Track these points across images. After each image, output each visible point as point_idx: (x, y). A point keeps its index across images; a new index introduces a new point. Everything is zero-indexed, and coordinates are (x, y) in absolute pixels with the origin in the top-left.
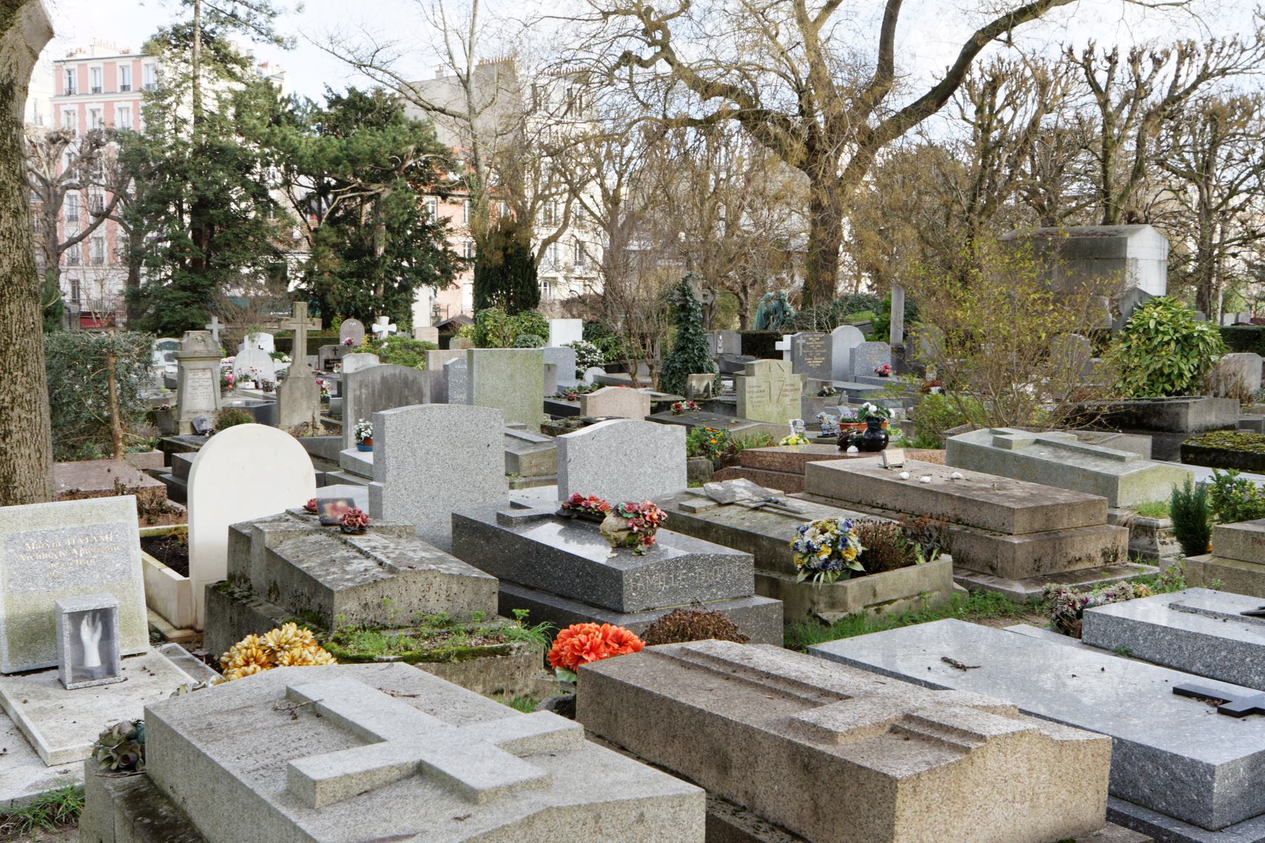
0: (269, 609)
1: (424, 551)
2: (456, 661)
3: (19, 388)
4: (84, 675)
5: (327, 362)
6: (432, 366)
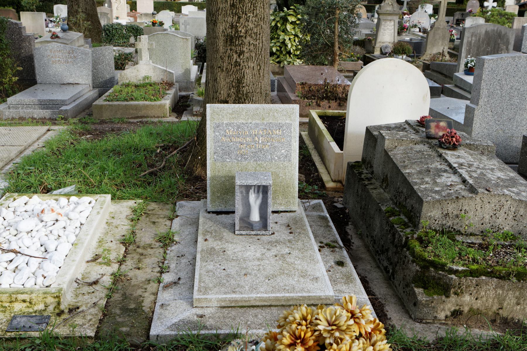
0: (380, 194)
1: (501, 170)
2: (515, 280)
3: (250, 24)
4: (248, 225)
5: (457, 20)
6: (515, 27)
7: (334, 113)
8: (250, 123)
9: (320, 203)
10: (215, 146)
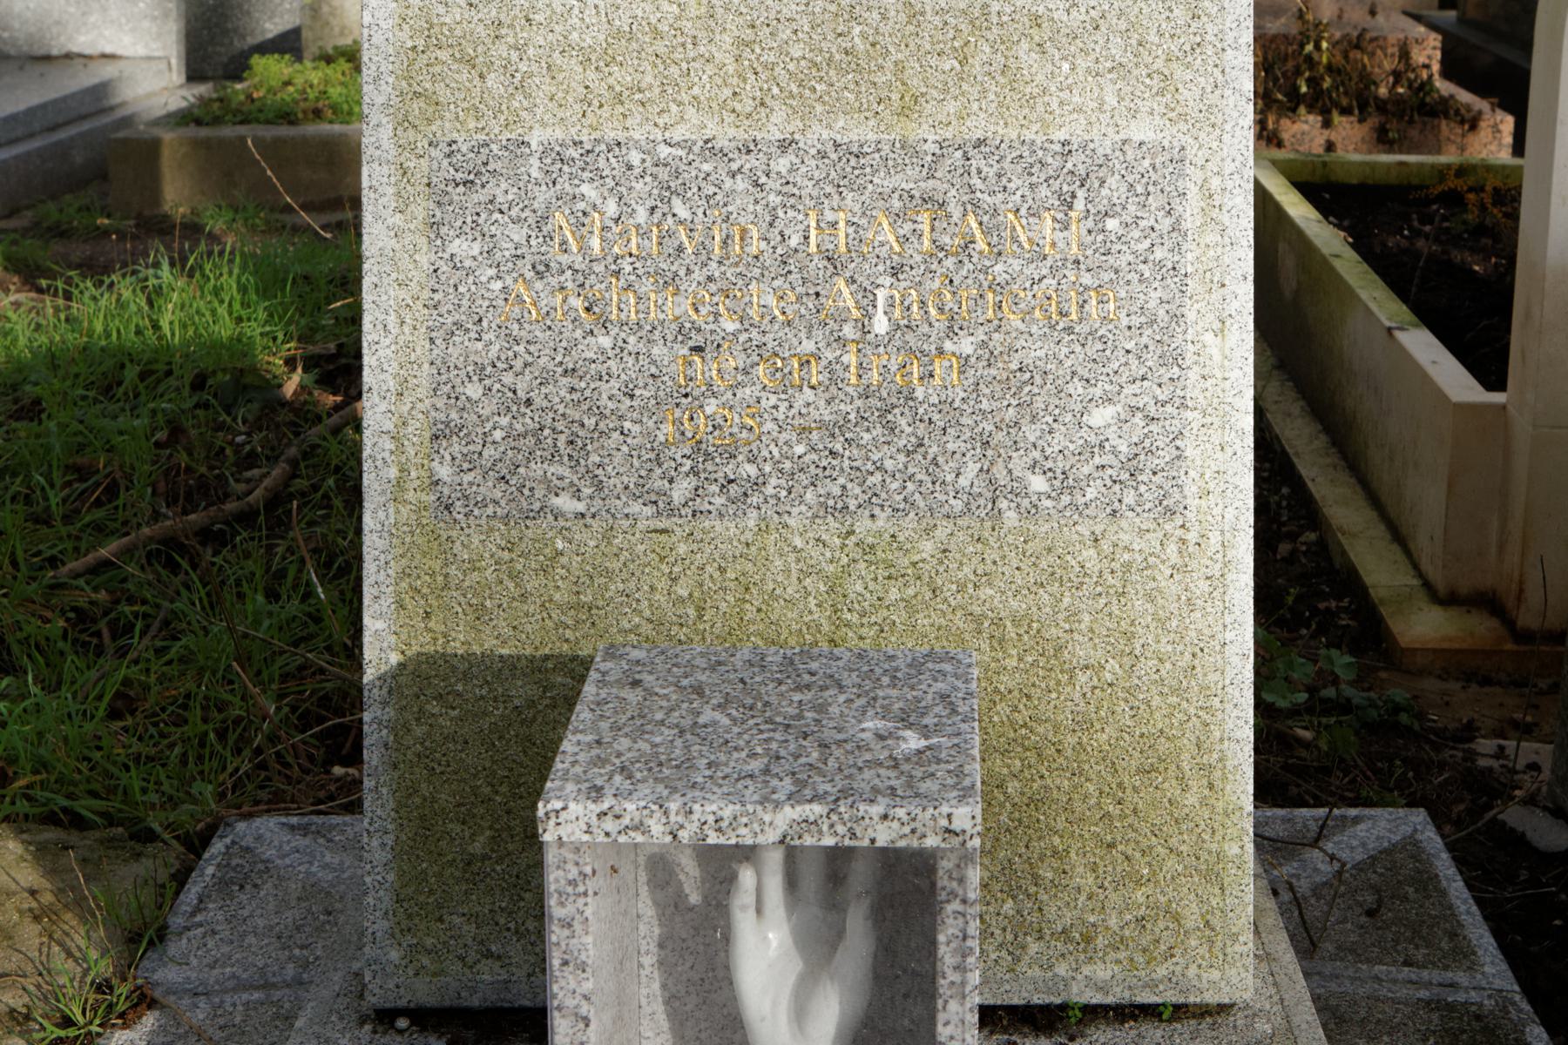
7: (1373, 166)
8: (785, 145)
9: (1411, 846)
10: (441, 366)
